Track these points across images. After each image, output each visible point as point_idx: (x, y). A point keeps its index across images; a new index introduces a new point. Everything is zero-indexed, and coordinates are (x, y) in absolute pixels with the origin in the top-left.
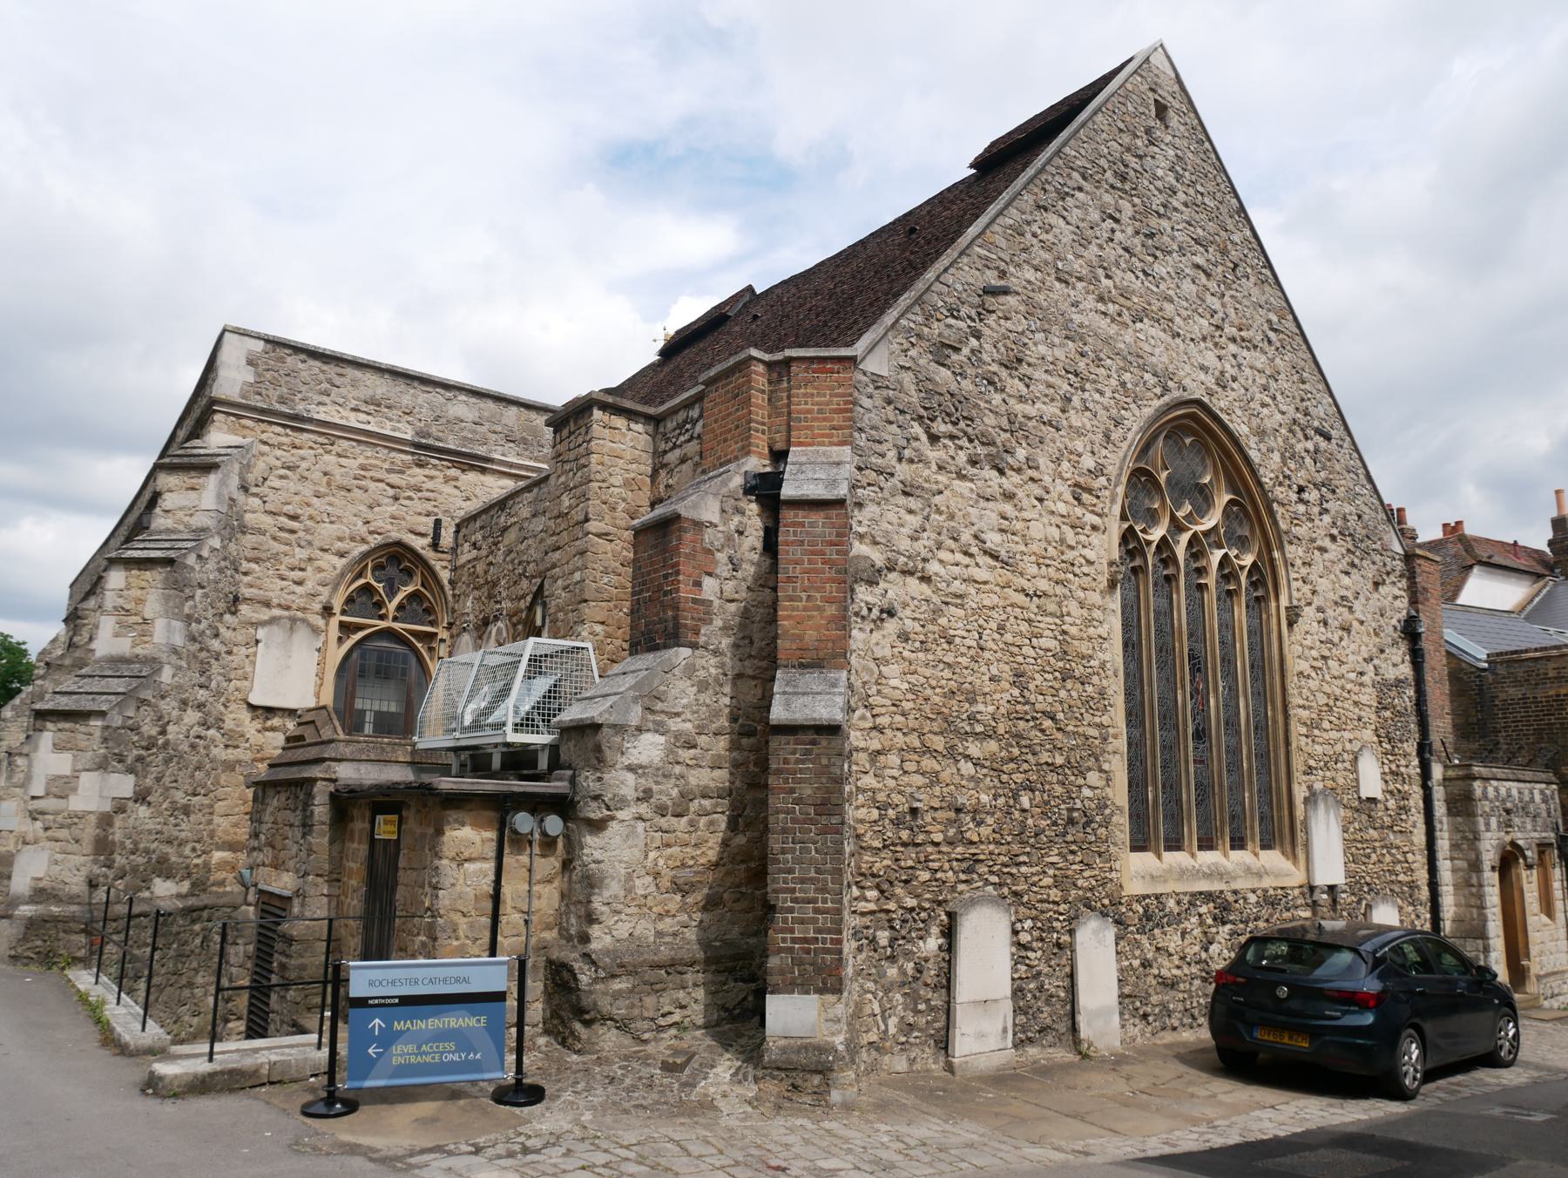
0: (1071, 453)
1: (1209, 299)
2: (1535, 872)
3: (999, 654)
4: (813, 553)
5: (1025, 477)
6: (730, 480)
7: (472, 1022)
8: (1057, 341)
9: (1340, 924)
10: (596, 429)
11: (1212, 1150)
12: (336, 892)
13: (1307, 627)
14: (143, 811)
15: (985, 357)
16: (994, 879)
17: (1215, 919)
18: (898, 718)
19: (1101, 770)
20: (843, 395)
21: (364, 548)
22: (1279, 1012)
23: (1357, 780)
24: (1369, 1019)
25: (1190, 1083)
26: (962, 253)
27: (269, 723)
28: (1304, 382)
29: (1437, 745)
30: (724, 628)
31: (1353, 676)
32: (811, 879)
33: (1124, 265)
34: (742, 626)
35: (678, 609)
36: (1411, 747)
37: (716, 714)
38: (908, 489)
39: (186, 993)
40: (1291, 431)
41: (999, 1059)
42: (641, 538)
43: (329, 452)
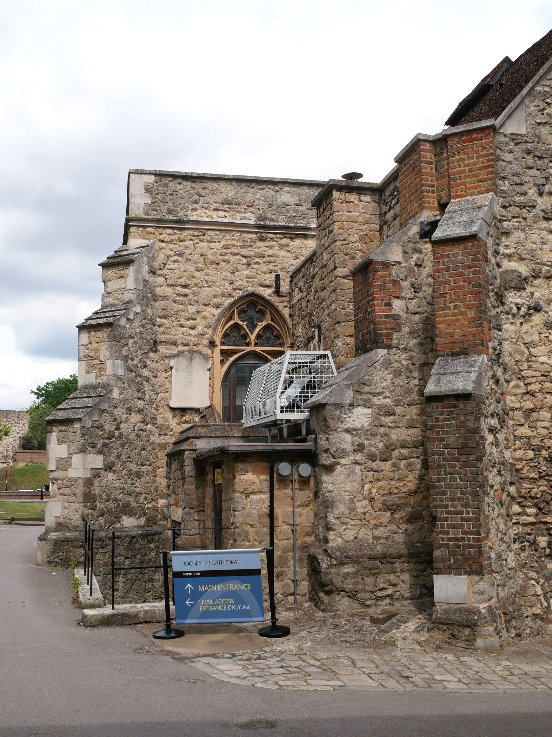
4: (457, 275)
6: (409, 230)
7: (242, 587)
10: (336, 205)
12: (203, 518)
14: (111, 476)
20: (487, 155)
21: (231, 300)
27: (184, 418)
30: (412, 333)
32: (458, 498)
35: (375, 323)
37: (409, 391)
39: (149, 585)
42: (356, 278)
43: (202, 241)
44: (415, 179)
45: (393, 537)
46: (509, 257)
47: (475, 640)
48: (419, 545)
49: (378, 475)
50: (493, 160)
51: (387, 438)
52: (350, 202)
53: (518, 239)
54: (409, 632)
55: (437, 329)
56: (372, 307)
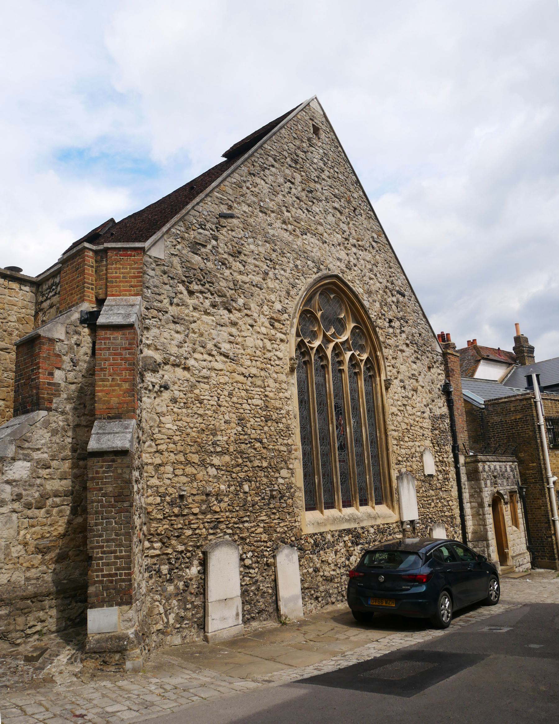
0: (268, 301)
1: (342, 225)
2: (509, 505)
3: (230, 409)
4: (115, 354)
5: (243, 314)
6: (72, 315)
8: (260, 243)
9: (417, 540)
11: (340, 670)
13: (395, 390)
15: (220, 250)
16: (230, 531)
17: (352, 543)
18: (171, 445)
19: (288, 469)
22: (382, 589)
23: (423, 466)
24: (423, 588)
25: (338, 632)
26: (207, 195)
28: (391, 268)
29: (461, 446)
30: (68, 399)
31: (419, 414)
32: (113, 540)
33: (296, 206)
34: (79, 398)
36: (449, 448)
37: (63, 448)
38: (176, 320)
40: (384, 292)
41: (234, 631)
42: (20, 349)
44: (78, 277)
45: (43, 577)
46: (148, 346)
47: (125, 663)
48: (65, 581)
49: (33, 522)
50: (142, 273)
51: (42, 488)
52: (12, 289)
53: (155, 334)
54: (63, 665)
55: (96, 397)
56: (36, 375)
